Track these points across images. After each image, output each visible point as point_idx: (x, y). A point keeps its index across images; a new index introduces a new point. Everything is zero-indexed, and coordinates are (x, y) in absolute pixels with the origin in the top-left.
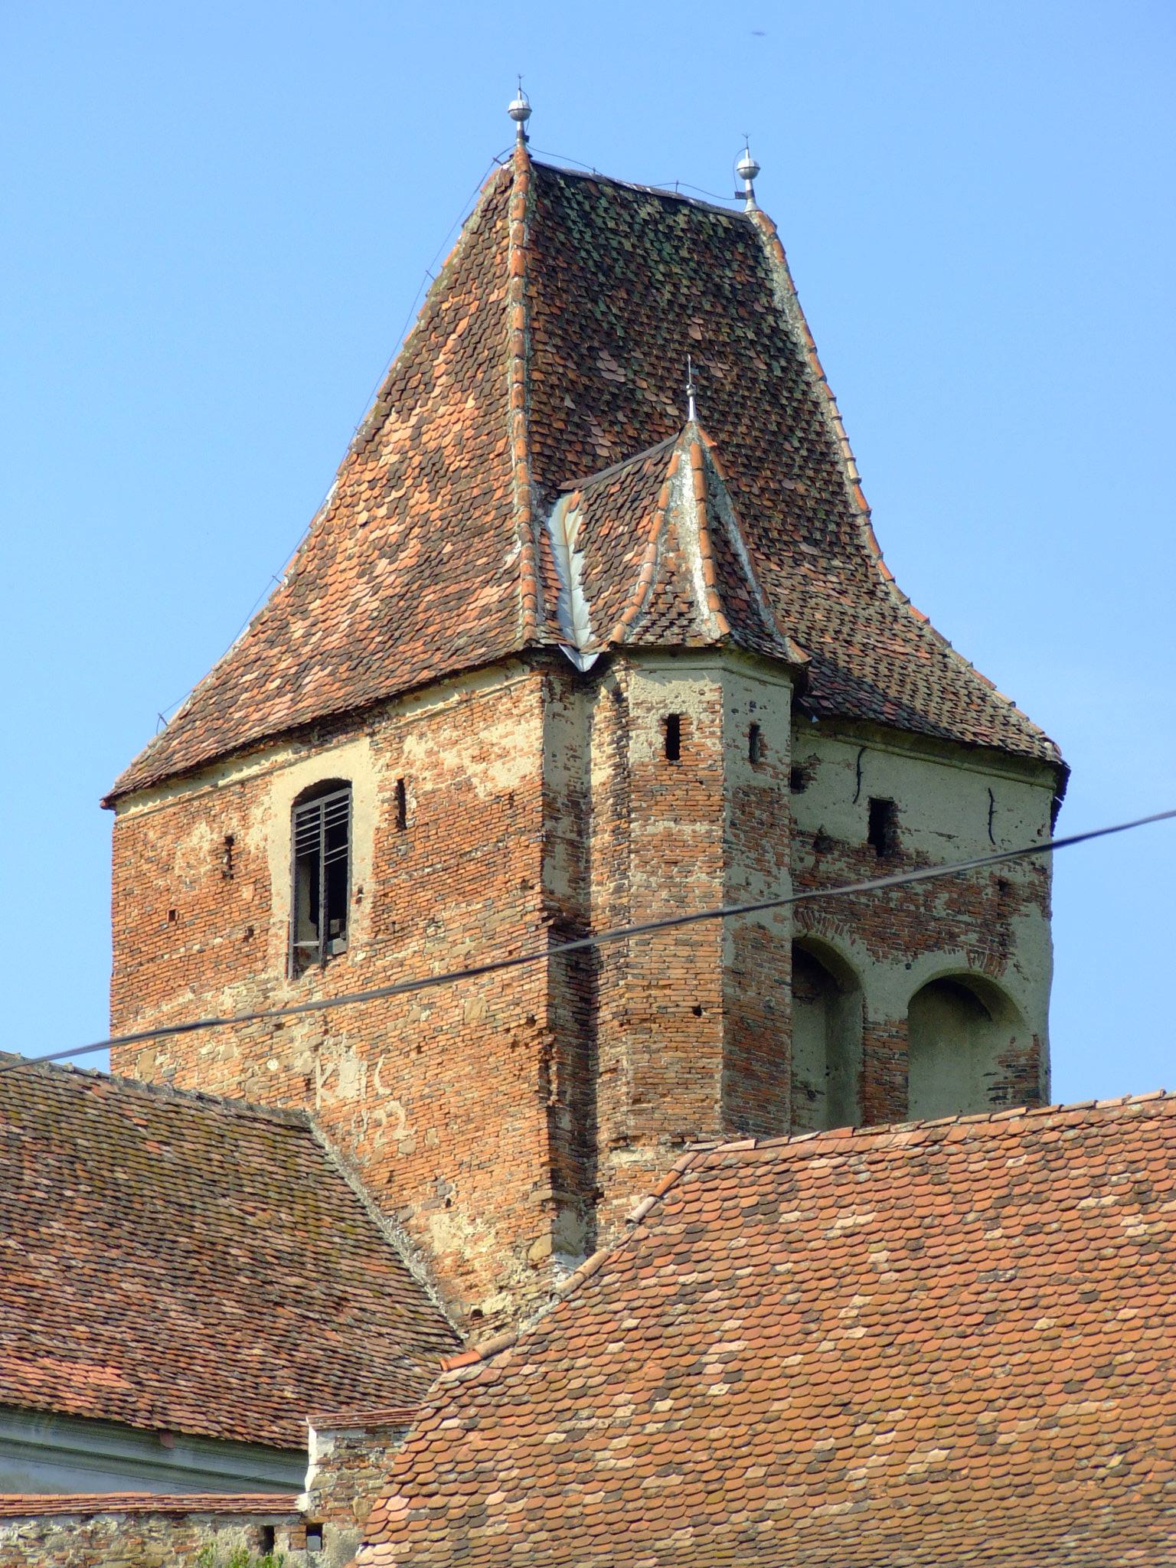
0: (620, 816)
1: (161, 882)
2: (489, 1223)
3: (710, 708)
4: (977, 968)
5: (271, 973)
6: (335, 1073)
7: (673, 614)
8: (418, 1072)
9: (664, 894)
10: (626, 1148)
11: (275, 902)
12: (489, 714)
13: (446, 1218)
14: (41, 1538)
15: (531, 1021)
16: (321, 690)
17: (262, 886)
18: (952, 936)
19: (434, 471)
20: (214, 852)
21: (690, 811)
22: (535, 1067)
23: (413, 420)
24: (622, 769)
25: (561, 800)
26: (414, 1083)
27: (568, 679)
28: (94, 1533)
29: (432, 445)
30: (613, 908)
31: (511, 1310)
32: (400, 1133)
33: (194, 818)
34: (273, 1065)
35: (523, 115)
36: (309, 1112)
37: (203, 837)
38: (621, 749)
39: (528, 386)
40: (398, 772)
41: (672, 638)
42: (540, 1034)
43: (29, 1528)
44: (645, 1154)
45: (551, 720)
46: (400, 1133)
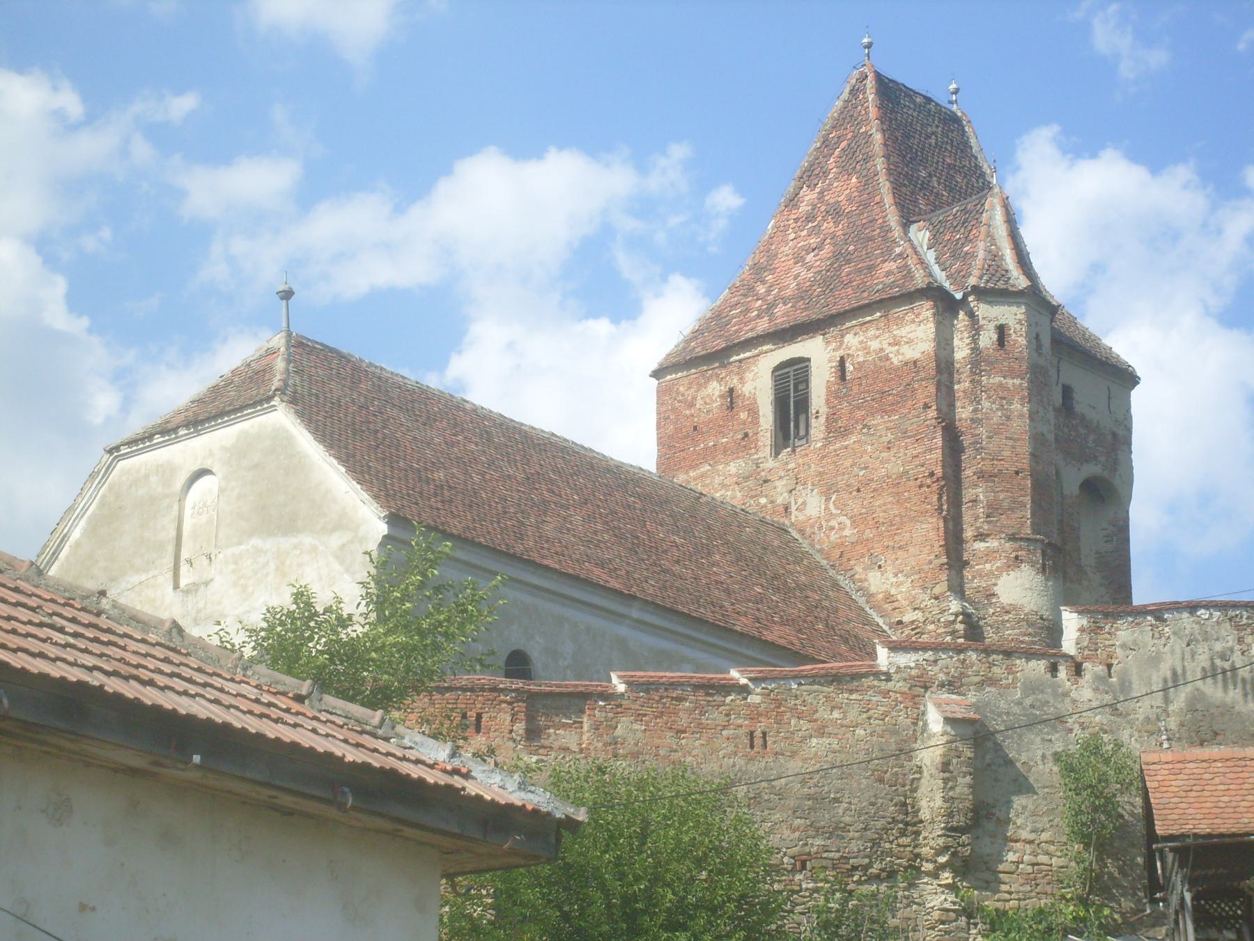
0: (975, 374)
1: (688, 412)
2: (907, 576)
3: (1020, 322)
4: (1106, 474)
5: (761, 455)
6: (804, 503)
7: (998, 275)
8: (859, 501)
9: (999, 414)
10: (983, 540)
11: (762, 420)
12: (900, 322)
13: (879, 574)
14: (935, 661)
15: (932, 474)
16: (783, 315)
17: (754, 412)
18: (1095, 457)
19: (836, 212)
20: (721, 396)
21: (1012, 373)
22: (935, 498)
23: (817, 190)
24: (975, 350)
25: (943, 365)
26: (855, 506)
27: (947, 306)
28: (965, 660)
29: (832, 201)
30: (972, 420)
31: (922, 620)
32: (847, 532)
33: (708, 380)
34: (763, 501)
35: (869, 46)
36: (787, 522)
37: (715, 389)
38: (975, 339)
39: (889, 172)
40: (841, 353)
41: (1001, 285)
42: (938, 480)
43: (929, 655)
44: (993, 543)
45: (938, 324)
46: (847, 532)
